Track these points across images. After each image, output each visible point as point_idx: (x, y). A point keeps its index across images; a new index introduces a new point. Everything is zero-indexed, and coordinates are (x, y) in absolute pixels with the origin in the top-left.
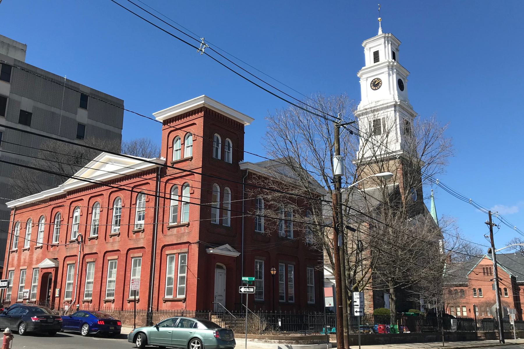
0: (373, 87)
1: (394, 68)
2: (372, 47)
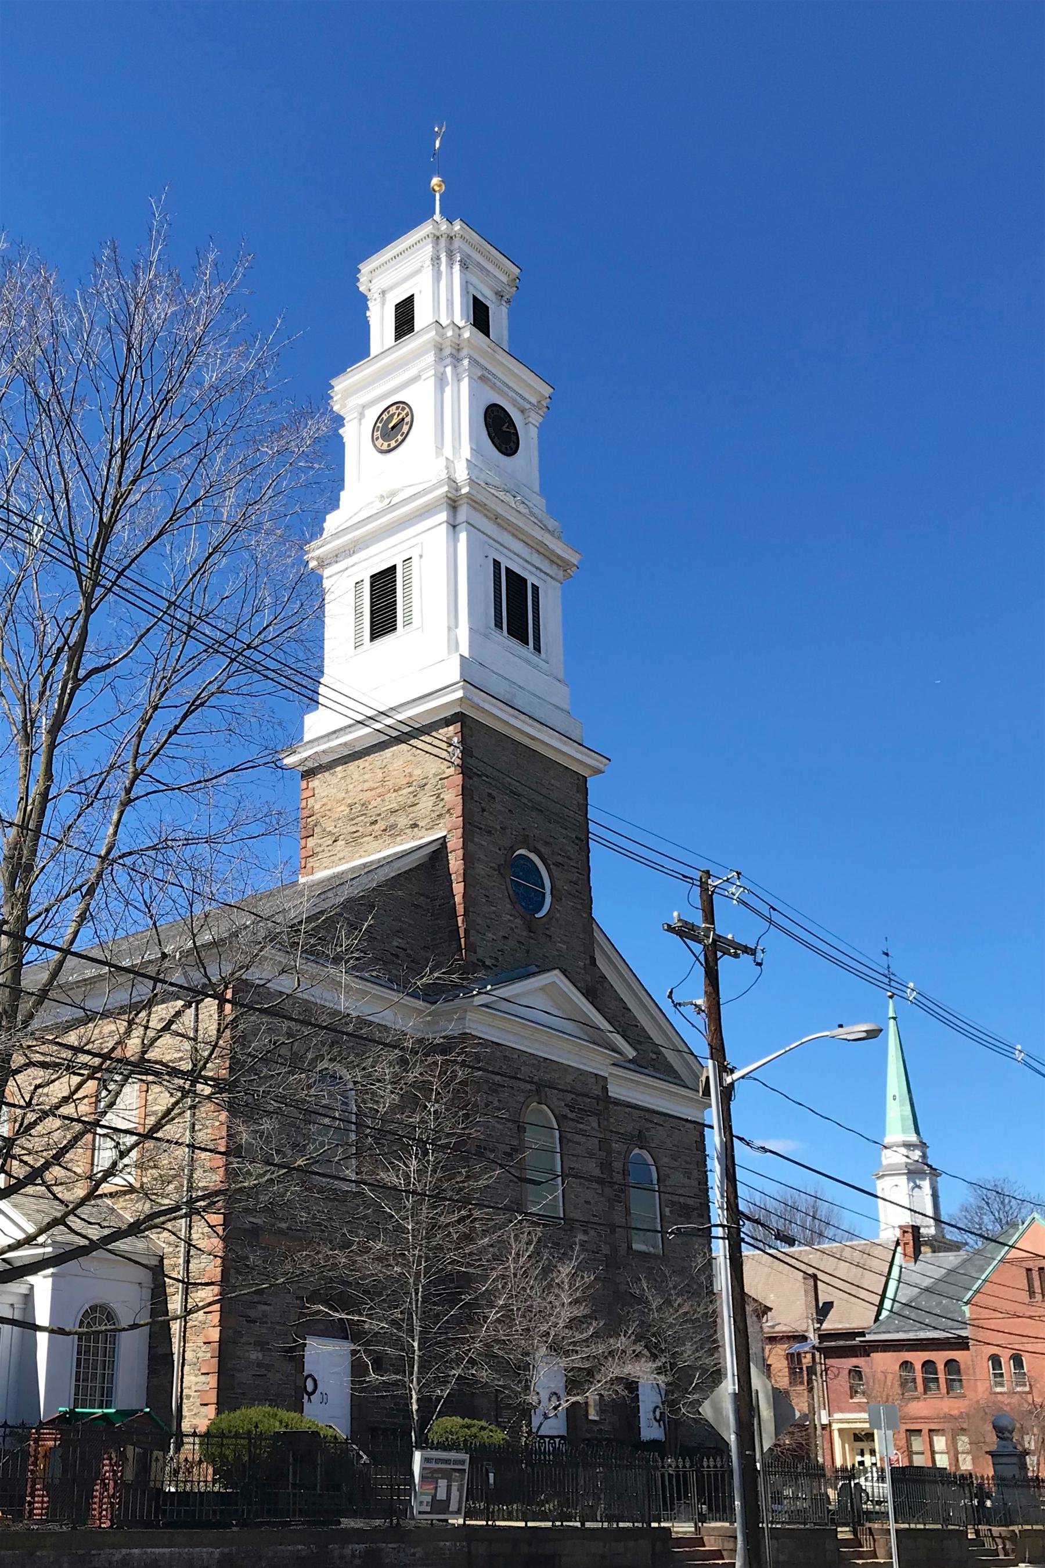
0: (378, 434)
1: (465, 352)
2: (392, 288)
